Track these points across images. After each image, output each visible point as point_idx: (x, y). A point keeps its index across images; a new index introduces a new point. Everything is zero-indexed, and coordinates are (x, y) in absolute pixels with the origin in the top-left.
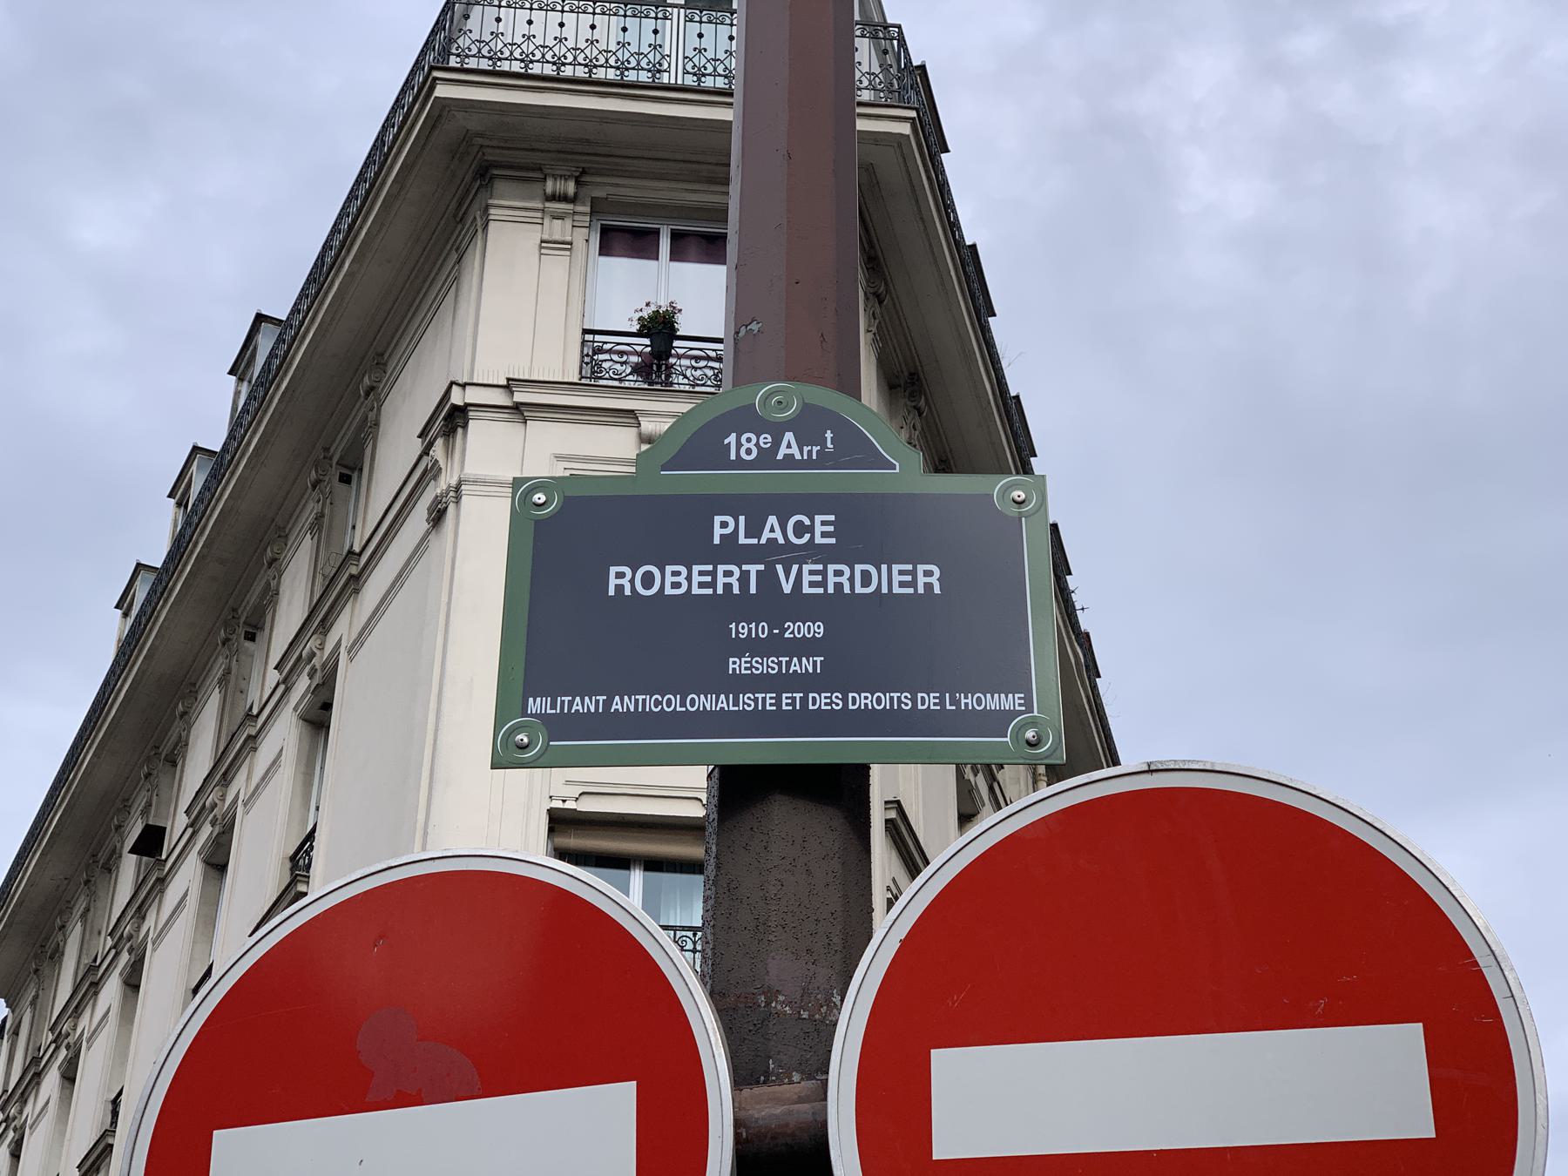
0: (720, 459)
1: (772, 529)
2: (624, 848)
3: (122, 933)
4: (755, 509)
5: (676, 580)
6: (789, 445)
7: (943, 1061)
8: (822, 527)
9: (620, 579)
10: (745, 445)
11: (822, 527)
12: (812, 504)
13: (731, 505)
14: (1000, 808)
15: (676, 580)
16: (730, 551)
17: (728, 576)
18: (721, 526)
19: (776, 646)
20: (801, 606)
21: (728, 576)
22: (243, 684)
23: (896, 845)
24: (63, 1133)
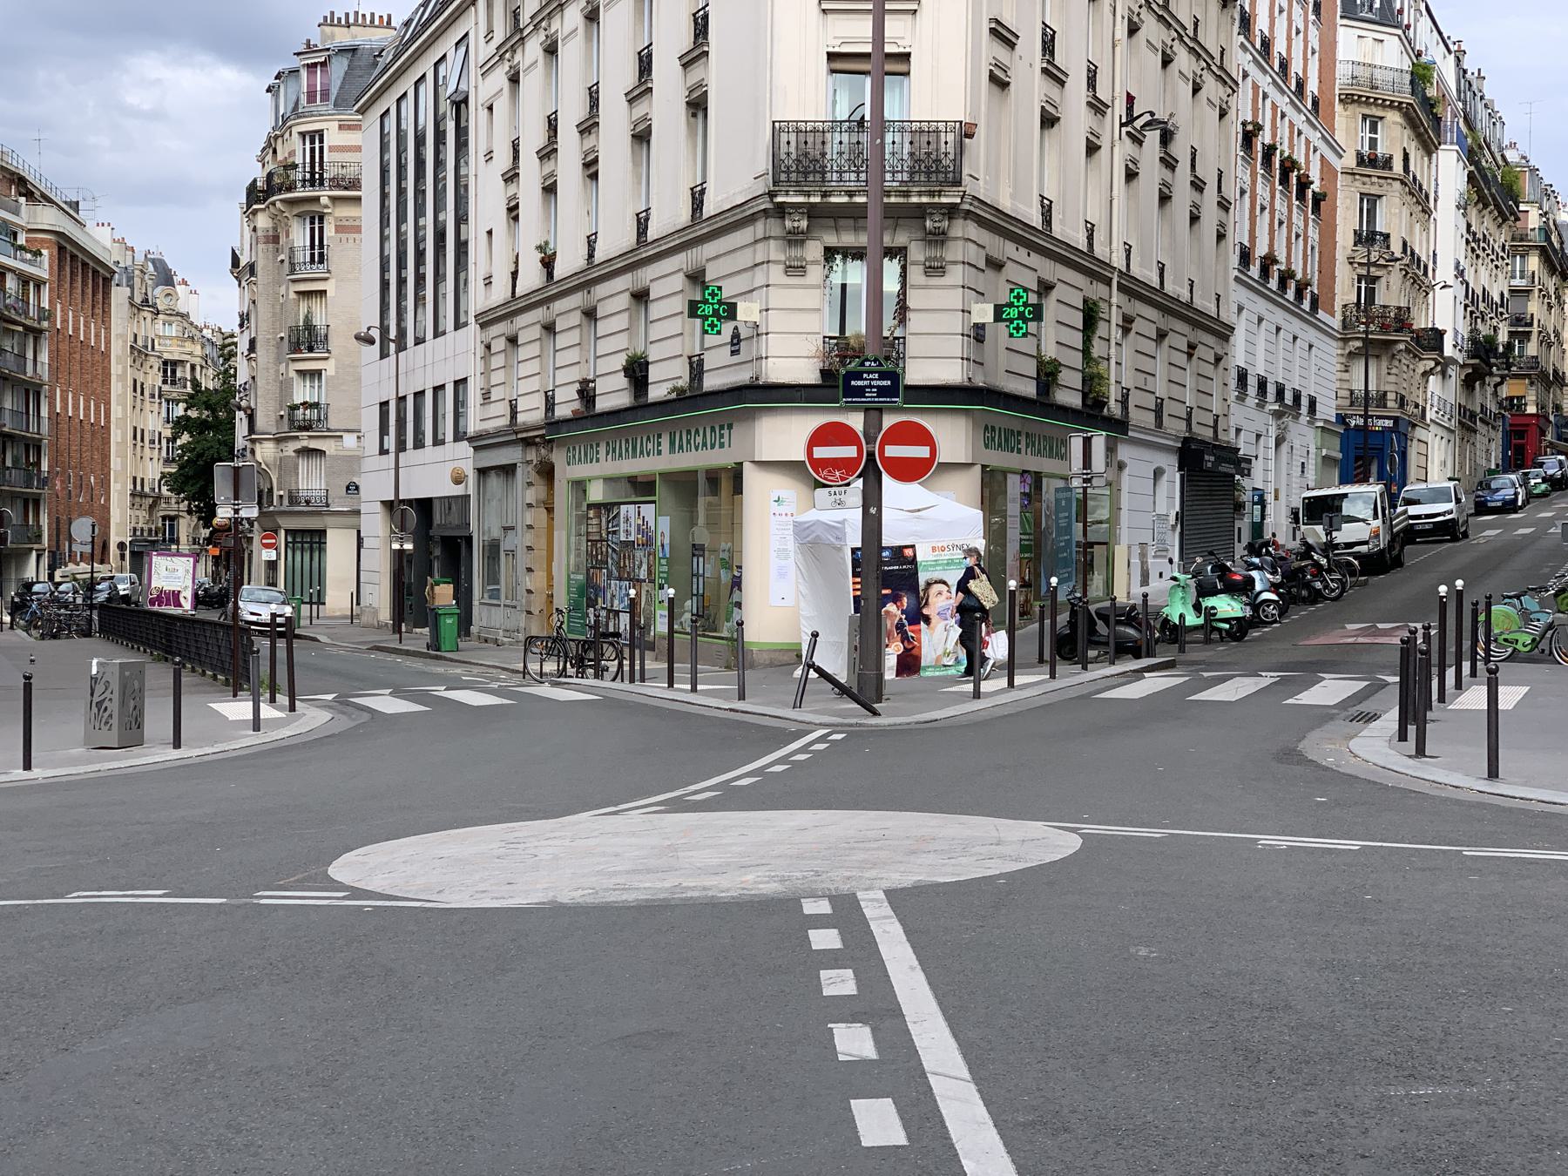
0: (864, 365)
1: (871, 376)
2: (611, 899)
3: (344, 898)
4: (869, 373)
5: (860, 383)
6: (873, 364)
7: (928, 456)
8: (877, 375)
9: (853, 383)
10: (867, 364)
11: (877, 375)
12: (875, 372)
13: (865, 372)
14: (358, 230)
15: (860, 383)
16: (866, 379)
17: (866, 383)
18: (865, 375)
19: (871, 392)
20: (874, 387)
21: (866, 383)
22: (855, 655)
23: (1369, 697)
24: (492, 119)
